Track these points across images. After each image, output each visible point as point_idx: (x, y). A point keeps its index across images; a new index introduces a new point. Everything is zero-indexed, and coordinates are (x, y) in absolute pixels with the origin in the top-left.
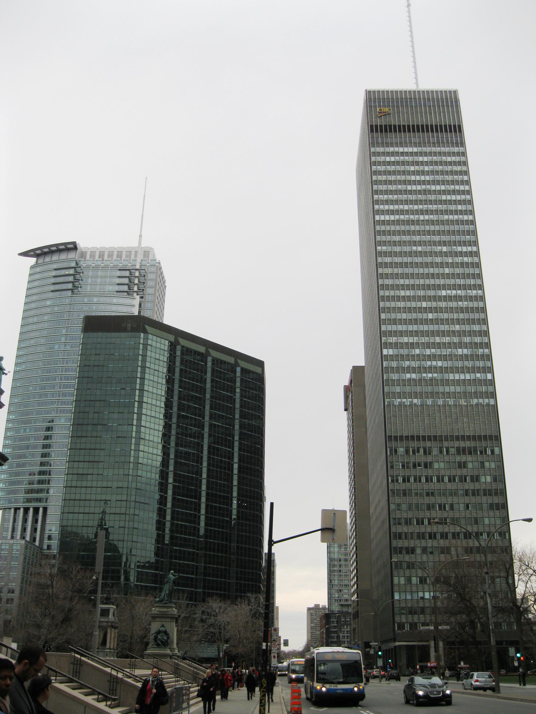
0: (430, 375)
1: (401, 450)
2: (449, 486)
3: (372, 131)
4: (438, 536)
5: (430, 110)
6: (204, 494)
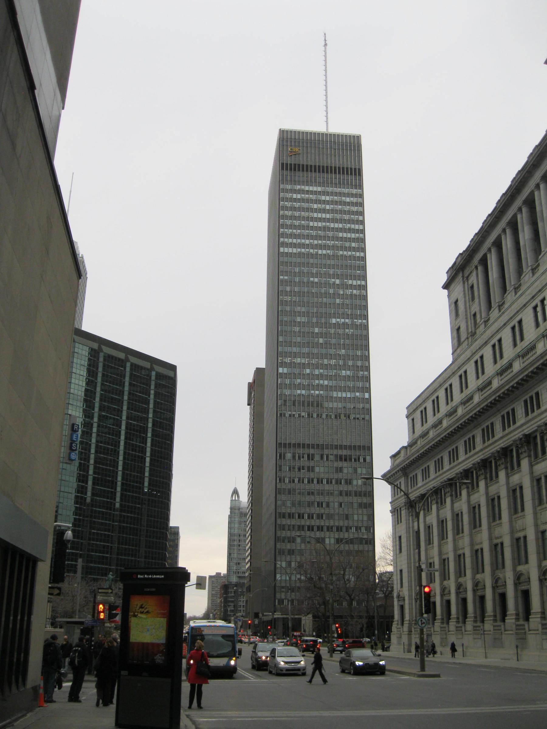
0: (317, 392)
1: (289, 456)
2: (327, 487)
3: (283, 169)
4: (315, 528)
5: (335, 153)
6: (119, 484)
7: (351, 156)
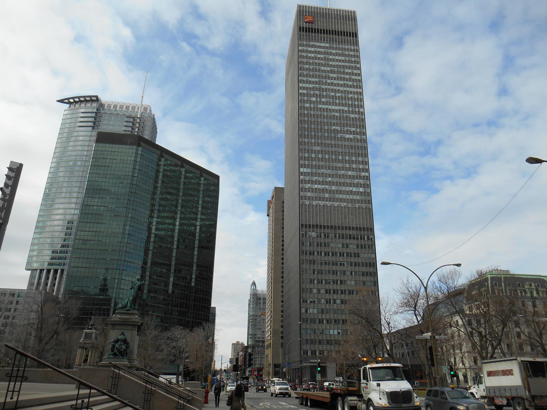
3: (300, 30)
5: (338, 22)
7: (349, 24)
